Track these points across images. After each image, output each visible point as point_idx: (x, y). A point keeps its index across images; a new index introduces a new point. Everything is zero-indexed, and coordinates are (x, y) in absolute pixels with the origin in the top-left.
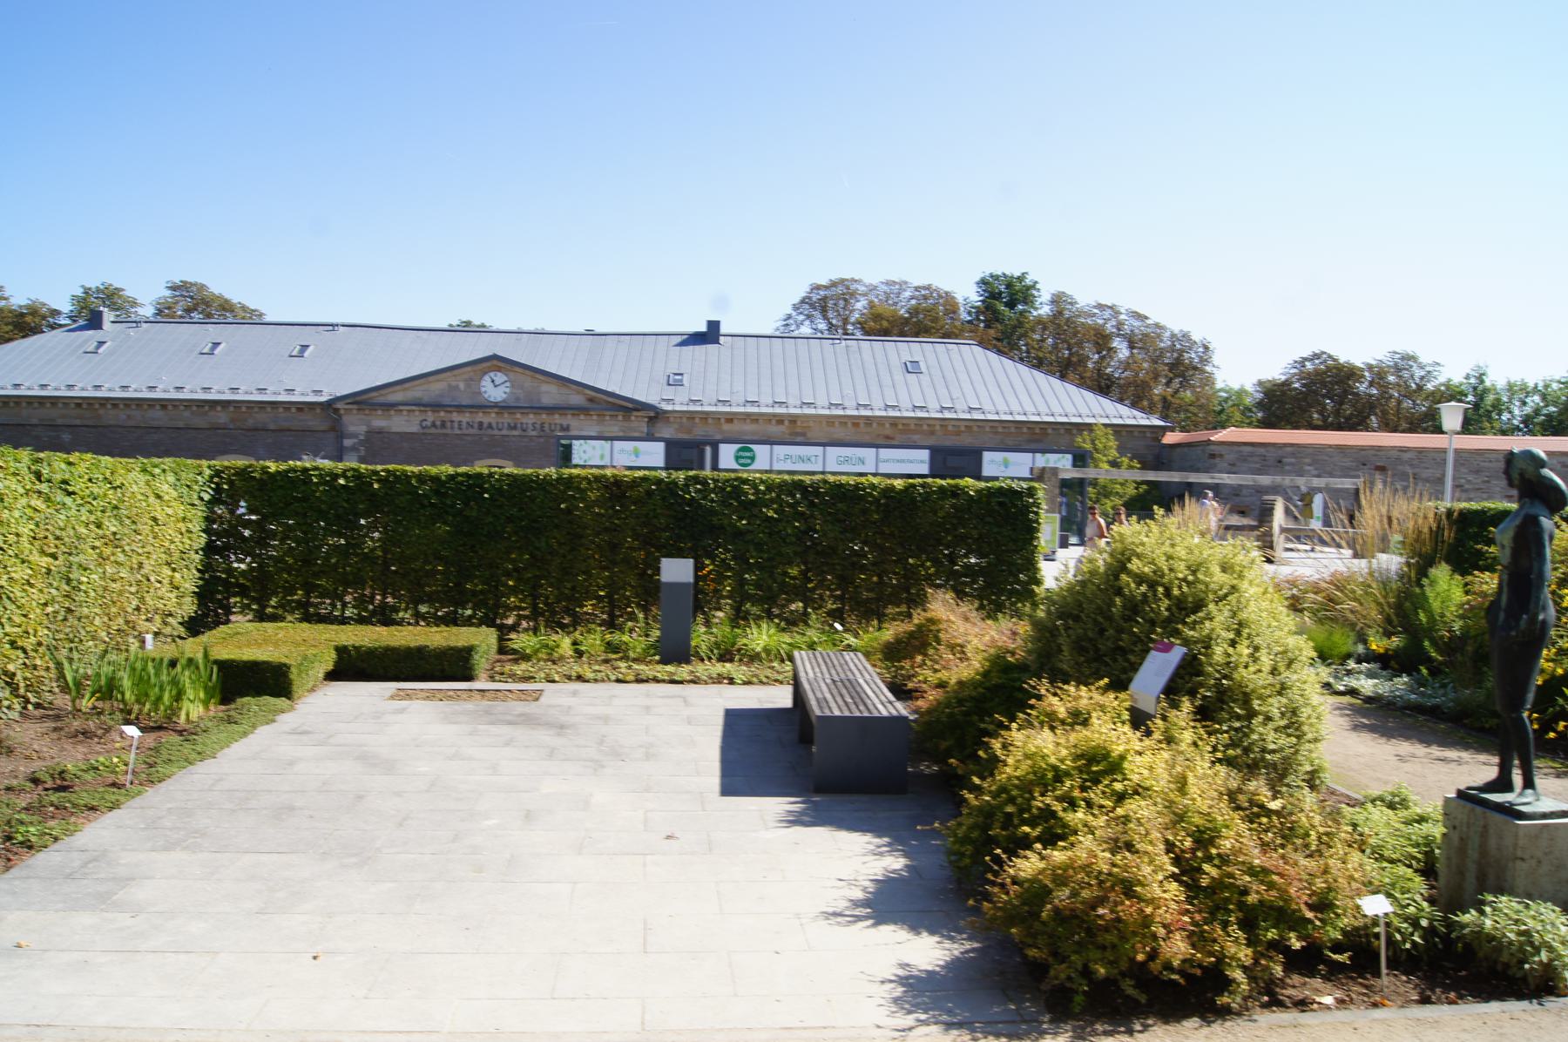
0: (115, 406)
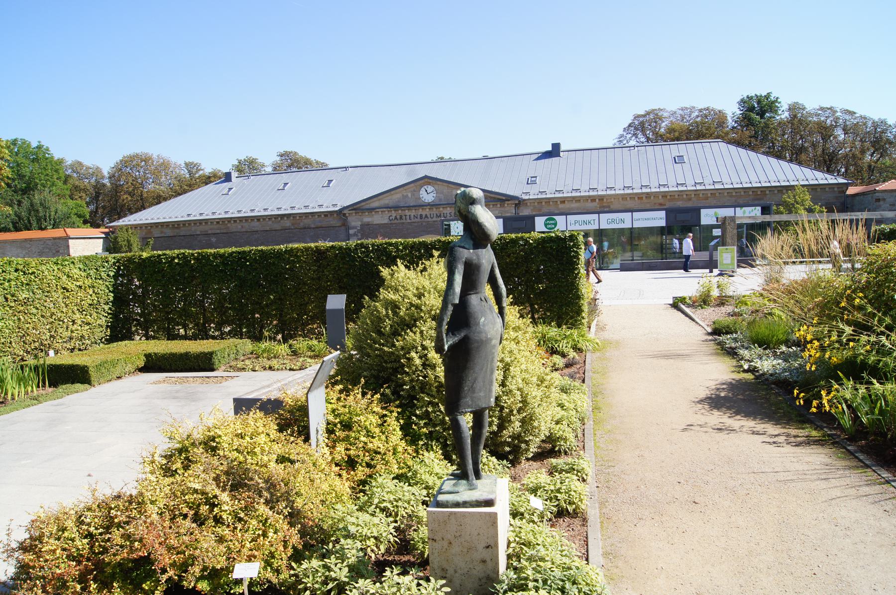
0: (326, 216)
